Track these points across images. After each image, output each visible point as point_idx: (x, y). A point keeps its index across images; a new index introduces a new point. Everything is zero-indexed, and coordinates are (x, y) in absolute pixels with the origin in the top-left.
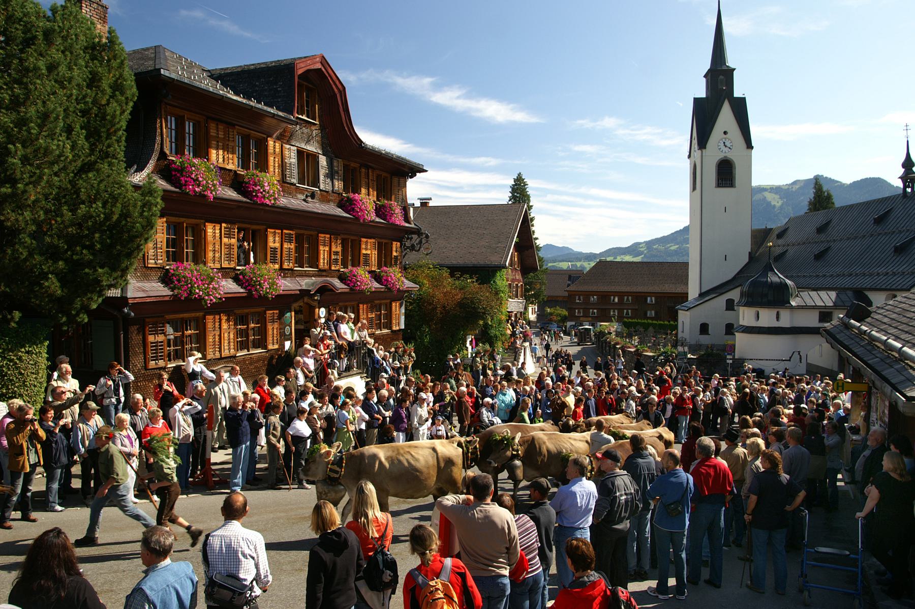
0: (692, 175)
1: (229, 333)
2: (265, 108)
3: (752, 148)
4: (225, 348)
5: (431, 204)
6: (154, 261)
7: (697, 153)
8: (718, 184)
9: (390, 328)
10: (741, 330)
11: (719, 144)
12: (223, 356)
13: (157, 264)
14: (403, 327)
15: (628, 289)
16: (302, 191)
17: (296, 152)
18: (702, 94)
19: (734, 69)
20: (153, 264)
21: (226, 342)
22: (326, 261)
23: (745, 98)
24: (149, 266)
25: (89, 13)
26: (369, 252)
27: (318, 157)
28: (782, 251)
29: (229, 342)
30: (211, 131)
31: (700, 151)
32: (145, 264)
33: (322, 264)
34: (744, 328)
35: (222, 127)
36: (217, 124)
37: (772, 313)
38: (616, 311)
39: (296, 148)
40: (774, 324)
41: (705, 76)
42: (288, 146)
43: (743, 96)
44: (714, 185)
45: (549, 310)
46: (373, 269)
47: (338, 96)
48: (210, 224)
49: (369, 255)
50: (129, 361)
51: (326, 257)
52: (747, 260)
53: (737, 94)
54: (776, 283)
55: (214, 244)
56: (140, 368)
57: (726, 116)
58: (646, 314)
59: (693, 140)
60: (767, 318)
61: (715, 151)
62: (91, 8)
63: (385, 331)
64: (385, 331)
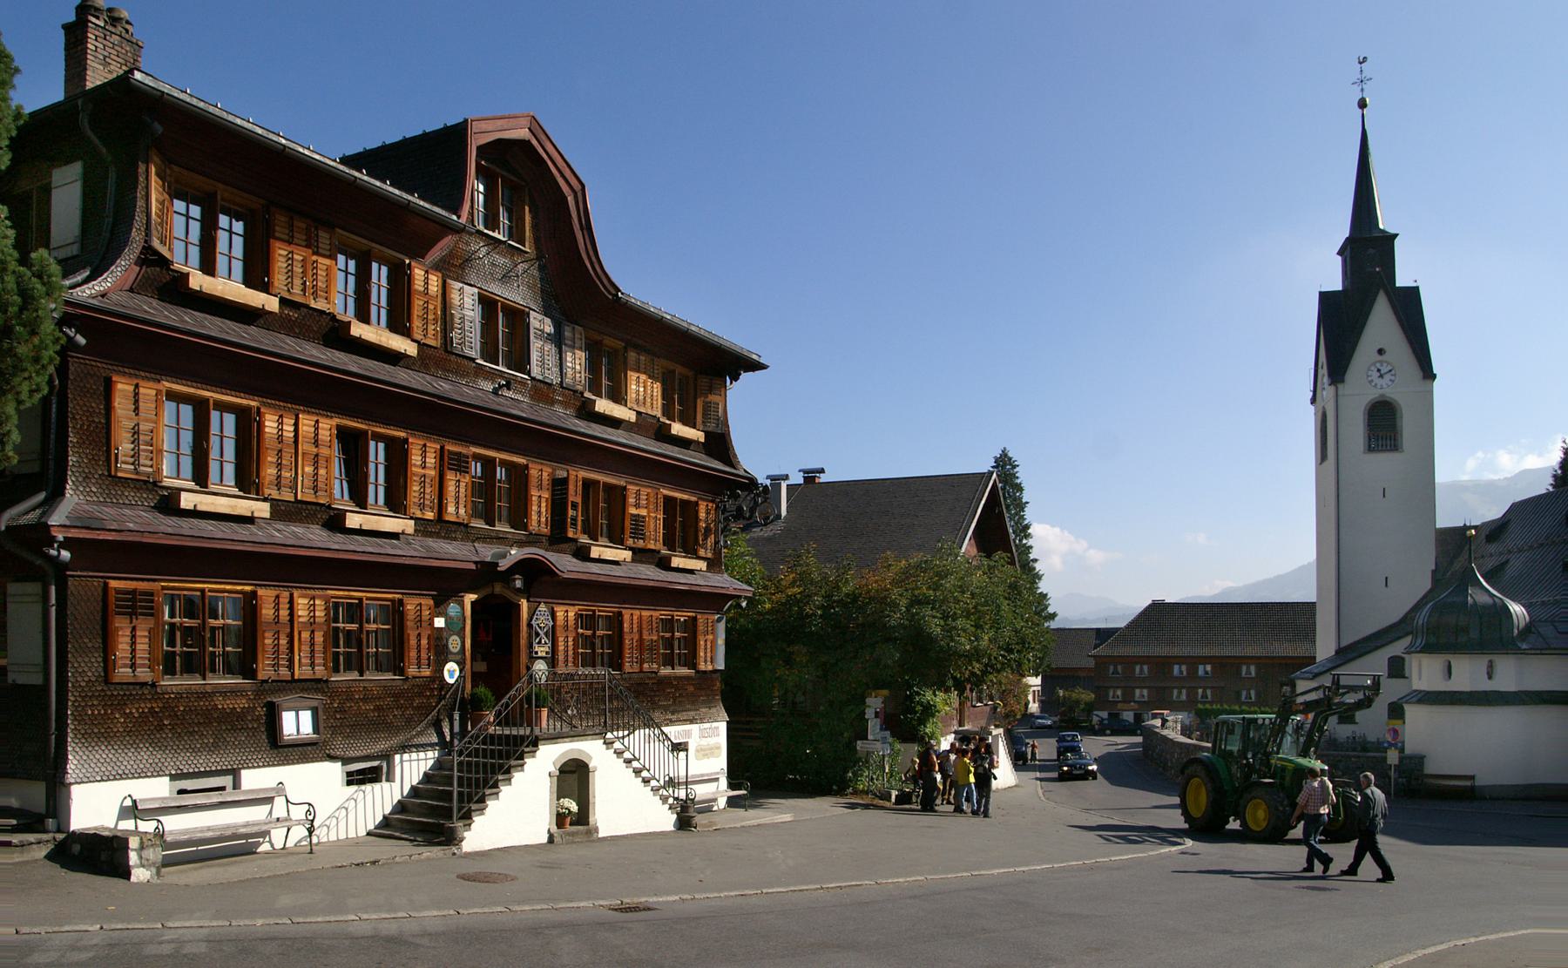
0: (1319, 445)
1: (313, 632)
2: (391, 189)
3: (1433, 377)
4: (303, 661)
5: (823, 478)
6: (132, 467)
7: (1328, 392)
8: (1370, 446)
9: (693, 666)
10: (1415, 699)
11: (1370, 373)
12: (296, 677)
13: (137, 473)
14: (721, 666)
15: (1206, 652)
16: (491, 375)
17: (477, 298)
18: (1336, 284)
19: (1397, 235)
20: (132, 473)
21: (306, 648)
22: (543, 519)
23: (1418, 288)
24: (119, 474)
25: (103, 52)
26: (643, 512)
27: (528, 314)
28: (1497, 563)
29: (312, 651)
30: (277, 228)
31: (1333, 387)
32: (109, 471)
33: (534, 523)
34: (1422, 694)
35: (304, 226)
36: (292, 218)
37: (1480, 663)
38: (1184, 691)
39: (476, 290)
40: (1485, 685)
41: (1339, 253)
42: (458, 285)
43: (1414, 285)
44: (1362, 449)
45: (1061, 693)
46: (652, 547)
47: (570, 199)
48: (272, 411)
49: (644, 517)
50: (68, 662)
51: (543, 510)
52: (1428, 585)
53: (1402, 280)
54: (1485, 607)
55: (280, 451)
56: (93, 679)
57: (1381, 324)
58: (1238, 694)
59: (1320, 370)
60: (1468, 673)
61: (1363, 386)
62: (105, 42)
63: (684, 671)
64: (684, 671)
